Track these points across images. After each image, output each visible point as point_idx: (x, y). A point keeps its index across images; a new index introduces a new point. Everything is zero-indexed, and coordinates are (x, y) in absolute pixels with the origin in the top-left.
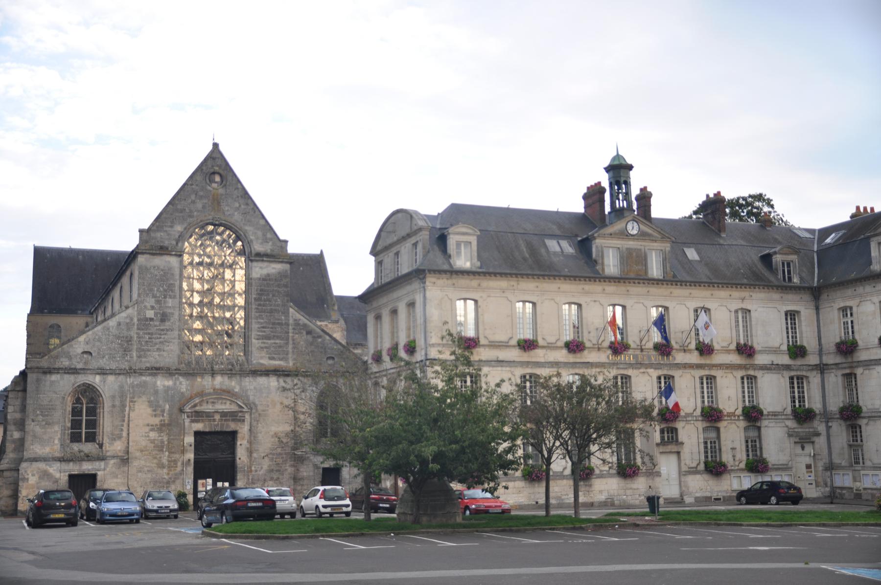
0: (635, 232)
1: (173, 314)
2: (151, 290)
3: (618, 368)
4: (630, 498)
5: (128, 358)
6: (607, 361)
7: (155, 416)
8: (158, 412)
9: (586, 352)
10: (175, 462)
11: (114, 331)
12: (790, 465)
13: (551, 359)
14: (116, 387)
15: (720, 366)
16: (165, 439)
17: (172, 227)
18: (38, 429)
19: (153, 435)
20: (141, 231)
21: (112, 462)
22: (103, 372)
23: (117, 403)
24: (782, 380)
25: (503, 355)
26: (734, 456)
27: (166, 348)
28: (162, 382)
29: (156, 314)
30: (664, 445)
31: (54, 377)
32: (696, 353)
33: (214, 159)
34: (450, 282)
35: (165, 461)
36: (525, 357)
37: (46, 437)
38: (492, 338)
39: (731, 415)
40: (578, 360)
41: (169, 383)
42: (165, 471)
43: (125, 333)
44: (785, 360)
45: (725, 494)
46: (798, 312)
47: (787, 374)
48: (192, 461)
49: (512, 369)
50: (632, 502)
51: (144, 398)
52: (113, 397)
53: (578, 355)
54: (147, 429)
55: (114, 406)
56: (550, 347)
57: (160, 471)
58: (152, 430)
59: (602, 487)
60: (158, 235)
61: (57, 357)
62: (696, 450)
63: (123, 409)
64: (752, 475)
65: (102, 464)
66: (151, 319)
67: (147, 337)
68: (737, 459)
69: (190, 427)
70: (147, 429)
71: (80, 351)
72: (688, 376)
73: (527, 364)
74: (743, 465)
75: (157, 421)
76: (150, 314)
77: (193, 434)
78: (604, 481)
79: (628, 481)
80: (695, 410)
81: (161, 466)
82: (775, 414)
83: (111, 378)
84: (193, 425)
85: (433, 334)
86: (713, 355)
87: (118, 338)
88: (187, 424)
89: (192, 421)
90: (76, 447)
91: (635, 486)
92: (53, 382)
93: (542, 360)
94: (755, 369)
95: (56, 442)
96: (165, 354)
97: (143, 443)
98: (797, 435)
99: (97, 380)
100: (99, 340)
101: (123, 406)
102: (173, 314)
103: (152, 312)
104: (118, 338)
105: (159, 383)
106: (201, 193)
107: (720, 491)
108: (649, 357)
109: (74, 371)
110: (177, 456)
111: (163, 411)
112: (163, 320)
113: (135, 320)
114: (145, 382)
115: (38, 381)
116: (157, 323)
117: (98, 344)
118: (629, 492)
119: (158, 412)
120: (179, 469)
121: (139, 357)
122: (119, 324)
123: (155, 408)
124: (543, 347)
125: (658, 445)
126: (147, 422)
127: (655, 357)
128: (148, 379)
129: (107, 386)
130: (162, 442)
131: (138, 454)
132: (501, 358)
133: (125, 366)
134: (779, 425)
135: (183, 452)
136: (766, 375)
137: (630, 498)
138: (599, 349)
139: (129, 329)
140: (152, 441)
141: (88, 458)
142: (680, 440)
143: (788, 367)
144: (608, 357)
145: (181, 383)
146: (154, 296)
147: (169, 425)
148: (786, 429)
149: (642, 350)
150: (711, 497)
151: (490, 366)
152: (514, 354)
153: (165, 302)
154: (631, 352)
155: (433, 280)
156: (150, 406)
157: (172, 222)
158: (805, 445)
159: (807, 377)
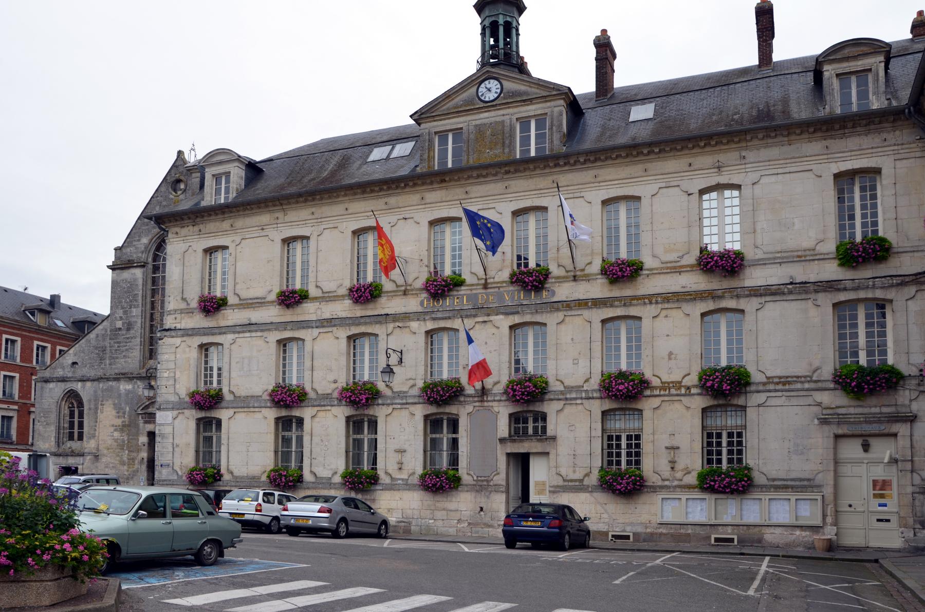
0: (491, 96)
1: (136, 322)
2: (121, 302)
3: (434, 319)
4: (440, 523)
5: (103, 366)
6: (420, 309)
7: (119, 417)
8: (121, 414)
9: (383, 300)
10: (133, 459)
11: (93, 342)
12: (817, 482)
13: (327, 315)
14: (92, 392)
15: (650, 299)
16: (126, 438)
17: (139, 240)
18: (41, 428)
19: (116, 434)
20: (116, 249)
21: (88, 458)
22: (82, 380)
23: (92, 406)
24: (813, 312)
25: (257, 316)
26: (673, 462)
27: (131, 355)
28: (125, 386)
29: (123, 324)
30: (514, 441)
31: (52, 385)
32: (602, 281)
33: (177, 167)
34: (196, 228)
35: (125, 459)
36: (289, 316)
37: (46, 435)
38: (244, 294)
39: (672, 389)
40: (370, 313)
41: (129, 387)
42: (126, 467)
43: (102, 344)
44: (832, 271)
45: (639, 529)
46: (877, 171)
47: (826, 300)
48: (146, 460)
49: (265, 334)
50: (442, 530)
51: (110, 402)
52: (90, 401)
53: (371, 306)
54: (112, 429)
55: (90, 409)
56: (328, 297)
57: (122, 468)
58: (115, 430)
59: (393, 505)
60: (128, 250)
61: (55, 368)
62: (583, 449)
63: (96, 413)
64: (710, 498)
65: (81, 458)
66: (120, 329)
67: (116, 345)
68: (680, 466)
69: (144, 427)
70: (112, 429)
71: (70, 362)
72: (578, 321)
73: (283, 326)
74: (692, 479)
75: (119, 422)
76: (119, 324)
77: (146, 434)
78: (397, 495)
79: (438, 498)
80: (587, 381)
81: (123, 463)
82: (785, 383)
83: (88, 384)
84: (147, 425)
85: (171, 298)
86: (640, 279)
87: (96, 348)
88: (141, 425)
89: (146, 422)
90: (69, 444)
91: (452, 505)
92: (51, 389)
93: (313, 317)
94: (738, 297)
95: (53, 439)
96: (129, 360)
97: (110, 442)
98: (841, 420)
99: (78, 387)
100: (83, 352)
101: (97, 409)
102: (136, 322)
103: (121, 322)
104: (96, 348)
105: (121, 387)
106: (164, 203)
107: (631, 524)
108: (500, 297)
109: (63, 380)
110: (134, 454)
111: (124, 413)
112: (128, 329)
113: (109, 332)
114: (112, 387)
115: (42, 388)
116: (124, 332)
117: (82, 355)
118: (439, 514)
119: (121, 414)
120: (136, 466)
121: (110, 364)
122: (97, 336)
123: (118, 409)
124: (315, 299)
125: (502, 440)
126: (112, 423)
127: (513, 296)
128: (114, 384)
129: (86, 391)
130: (123, 441)
131: (105, 452)
132: (254, 321)
133: (100, 373)
134: (795, 401)
135: (139, 451)
136: (770, 306)
137: (440, 523)
138: (405, 293)
139: (104, 340)
140: (116, 440)
141: (73, 454)
142: (550, 432)
143: (830, 286)
144: (422, 304)
145: (138, 387)
146: (123, 308)
147: (129, 426)
148: (816, 409)
149: (485, 286)
150: (606, 534)
151: (234, 332)
152: (273, 313)
153: (131, 312)
154: (463, 290)
155: (177, 229)
156: (115, 409)
157: (140, 236)
158: (873, 442)
159: (891, 301)
